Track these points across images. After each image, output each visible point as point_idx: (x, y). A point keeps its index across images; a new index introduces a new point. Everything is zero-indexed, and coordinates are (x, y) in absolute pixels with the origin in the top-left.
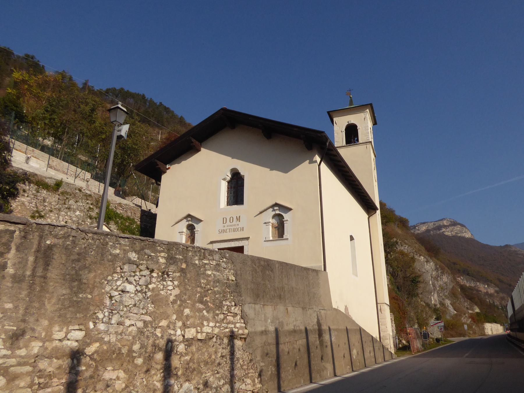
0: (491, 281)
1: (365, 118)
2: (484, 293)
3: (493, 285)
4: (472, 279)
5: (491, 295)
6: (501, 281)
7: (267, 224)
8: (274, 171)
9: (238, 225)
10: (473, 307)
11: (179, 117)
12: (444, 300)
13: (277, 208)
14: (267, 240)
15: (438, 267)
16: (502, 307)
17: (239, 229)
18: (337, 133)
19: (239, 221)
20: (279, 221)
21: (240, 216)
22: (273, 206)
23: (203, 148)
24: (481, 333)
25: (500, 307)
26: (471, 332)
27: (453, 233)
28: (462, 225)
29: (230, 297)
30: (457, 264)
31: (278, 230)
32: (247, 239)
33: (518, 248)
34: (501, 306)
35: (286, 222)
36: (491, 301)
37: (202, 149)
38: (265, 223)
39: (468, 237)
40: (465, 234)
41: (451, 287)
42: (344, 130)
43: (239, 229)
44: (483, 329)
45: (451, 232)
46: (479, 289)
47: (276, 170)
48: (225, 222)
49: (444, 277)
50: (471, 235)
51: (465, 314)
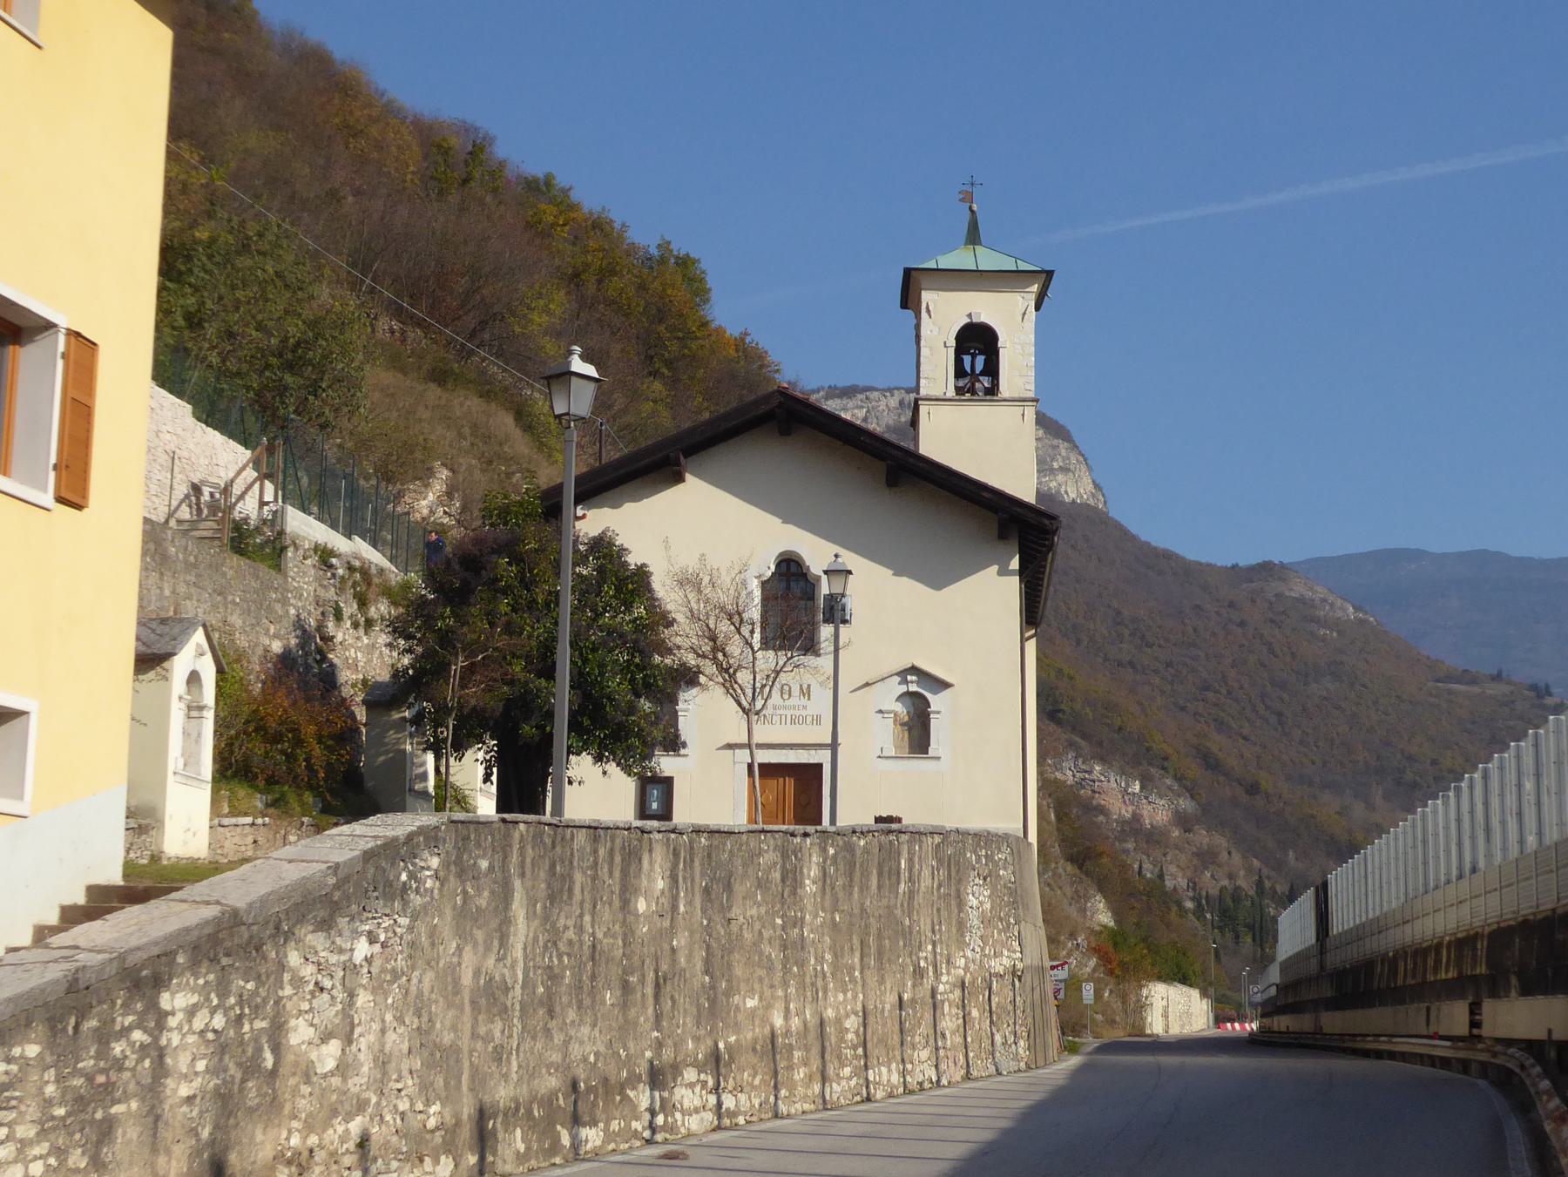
0: (1166, 759)
1: (1024, 314)
2: (1123, 822)
3: (1168, 782)
4: (1071, 745)
5: (1152, 838)
6: (1210, 763)
7: (886, 715)
8: (905, 579)
10: (1087, 898)
13: (914, 678)
14: (885, 754)
16: (1199, 905)
17: (809, 719)
19: (809, 699)
21: (809, 686)
25: (1189, 905)
26: (1099, 1017)
29: (588, 868)
31: (910, 731)
33: (1319, 589)
34: (1193, 899)
35: (936, 716)
36: (1147, 866)
37: (688, 476)
38: (880, 712)
40: (1060, 477)
43: (809, 719)
44: (1141, 1007)
46: (1099, 800)
47: (909, 577)
50: (1090, 487)
51: (1073, 936)
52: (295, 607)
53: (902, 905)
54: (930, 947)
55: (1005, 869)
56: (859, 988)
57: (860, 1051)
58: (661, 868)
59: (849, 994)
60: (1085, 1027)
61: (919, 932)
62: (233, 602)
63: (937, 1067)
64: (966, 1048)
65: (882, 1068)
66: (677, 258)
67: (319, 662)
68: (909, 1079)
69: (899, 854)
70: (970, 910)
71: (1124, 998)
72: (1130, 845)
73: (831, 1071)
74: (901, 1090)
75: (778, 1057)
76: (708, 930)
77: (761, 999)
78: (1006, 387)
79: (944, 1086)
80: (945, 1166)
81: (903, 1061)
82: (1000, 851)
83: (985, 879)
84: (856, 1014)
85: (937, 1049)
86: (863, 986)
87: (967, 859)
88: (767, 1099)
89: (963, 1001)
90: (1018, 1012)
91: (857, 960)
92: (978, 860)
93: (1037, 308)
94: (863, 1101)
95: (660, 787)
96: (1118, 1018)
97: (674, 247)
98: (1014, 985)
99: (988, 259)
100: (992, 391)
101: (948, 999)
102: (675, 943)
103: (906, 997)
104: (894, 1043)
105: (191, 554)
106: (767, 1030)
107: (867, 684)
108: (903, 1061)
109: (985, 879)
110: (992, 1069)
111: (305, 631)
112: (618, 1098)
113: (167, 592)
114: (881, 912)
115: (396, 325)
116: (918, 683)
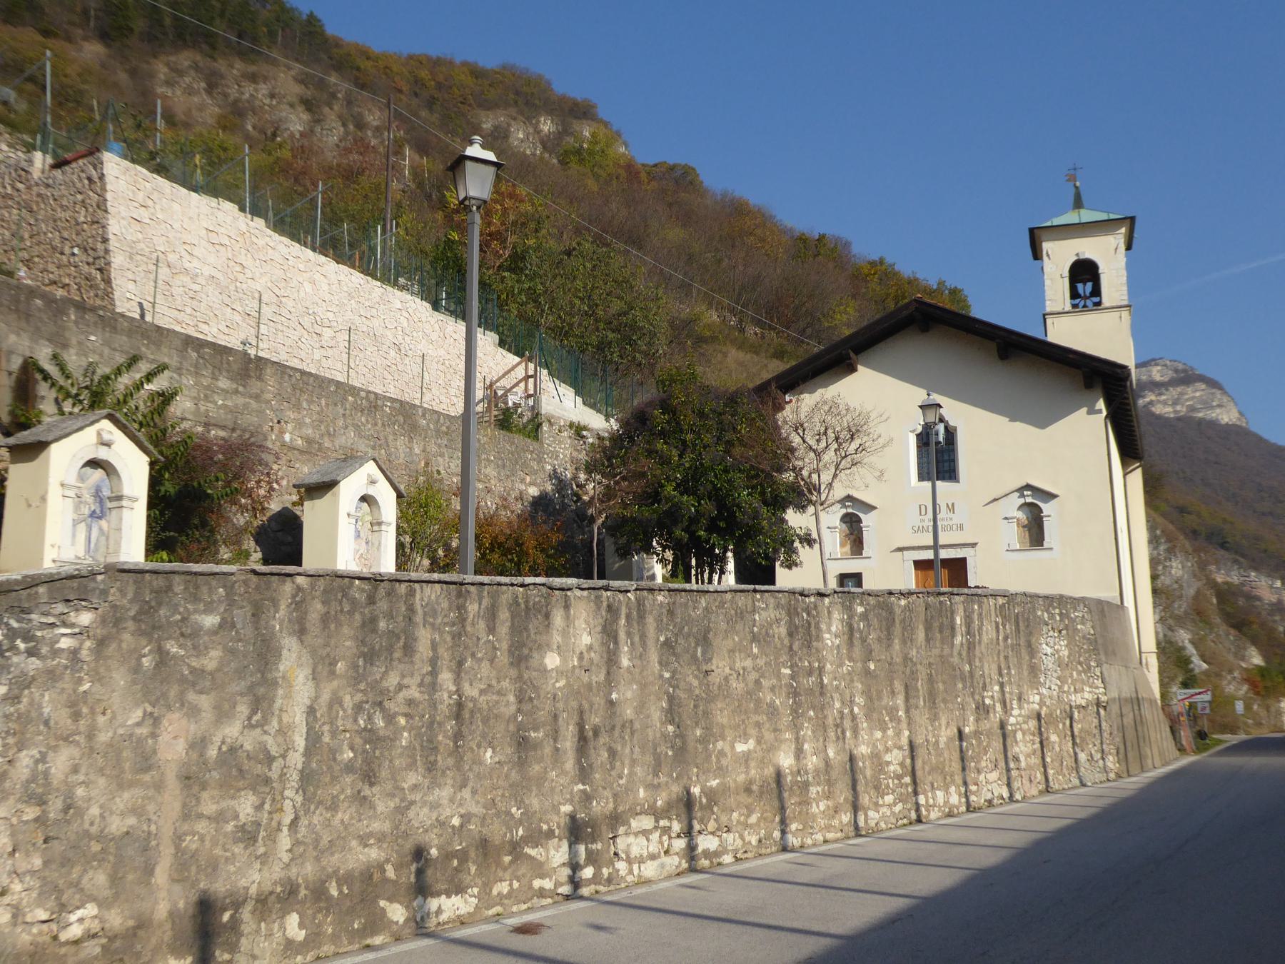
2: (1272, 604)
4: (1235, 561)
8: (1018, 423)
9: (951, 519)
10: (1245, 649)
11: (305, 17)
12: (1172, 631)
13: (1029, 493)
15: (1158, 532)
17: (955, 527)
18: (1051, 279)
20: (1030, 515)
21: (953, 504)
22: (1021, 490)
23: (862, 365)
24: (1275, 726)
26: (1250, 721)
27: (1178, 408)
28: (1213, 384)
30: (1189, 513)
32: (973, 545)
37: (859, 367)
38: (1006, 518)
39: (1227, 424)
40: (1218, 411)
41: (1192, 592)
42: (1066, 274)
43: (955, 527)
45: (1175, 403)
46: (1255, 592)
48: (923, 513)
49: (1174, 564)
50: (1237, 415)
51: (1230, 672)
52: (550, 464)
53: (960, 654)
54: (997, 688)
55: (1083, 624)
56: (904, 725)
57: (907, 780)
58: (587, 622)
59: (890, 732)
60: (1239, 728)
61: (983, 676)
62: (488, 460)
63: (1009, 785)
64: (1045, 767)
65: (938, 793)
66: (950, 290)
67: (576, 502)
68: (973, 798)
69: (953, 613)
70: (1044, 657)
71: (1268, 708)
72: (1277, 618)
73: (865, 800)
74: (963, 809)
75: (786, 795)
76: (674, 682)
77: (759, 742)
78: (1107, 299)
79: (1017, 801)
80: (812, 946)
81: (965, 784)
82: (1075, 610)
83: (1060, 632)
84: (900, 748)
85: (1008, 770)
86: (909, 724)
87: (1039, 617)
88: (769, 836)
89: (1040, 729)
90: (1106, 735)
91: (900, 701)
92: (1052, 616)
93: (1129, 247)
94: (910, 823)
95: (853, 580)
96: (1264, 722)
97: (948, 284)
98: (1098, 713)
99: (1087, 216)
100: (1099, 304)
101: (1021, 729)
102: (614, 696)
103: (967, 730)
104: (952, 769)
105: (442, 425)
106: (769, 771)
107: (995, 500)
108: (965, 784)
109: (1060, 632)
110: (1077, 782)
111: (561, 481)
112: (507, 859)
113: (417, 451)
114: (932, 660)
115: (758, 330)
116: (1032, 496)
